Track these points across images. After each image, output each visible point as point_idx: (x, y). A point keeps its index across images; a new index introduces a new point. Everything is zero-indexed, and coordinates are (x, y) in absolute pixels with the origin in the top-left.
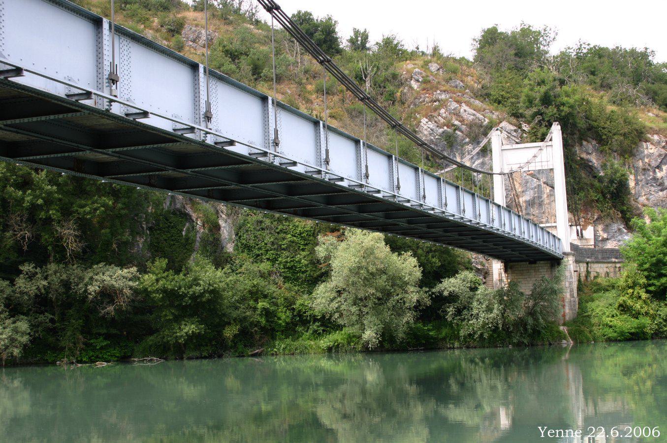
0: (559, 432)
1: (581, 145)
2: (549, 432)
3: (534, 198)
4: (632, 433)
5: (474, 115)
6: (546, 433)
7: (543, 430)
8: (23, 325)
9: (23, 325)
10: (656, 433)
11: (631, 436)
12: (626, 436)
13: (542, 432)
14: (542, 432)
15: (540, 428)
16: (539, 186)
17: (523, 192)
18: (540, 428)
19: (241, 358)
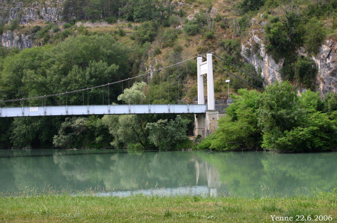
0: (281, 218)
1: (300, 49)
2: (276, 218)
3: (273, 78)
4: (318, 219)
5: (276, 26)
6: (274, 219)
7: (273, 217)
8: (233, 47)
9: (233, 47)
10: (330, 219)
11: (303, 220)
12: (301, 220)
13: (273, 218)
14: (273, 218)
15: (271, 216)
16: (274, 72)
17: (269, 76)
18: (271, 216)
19: (261, 152)
